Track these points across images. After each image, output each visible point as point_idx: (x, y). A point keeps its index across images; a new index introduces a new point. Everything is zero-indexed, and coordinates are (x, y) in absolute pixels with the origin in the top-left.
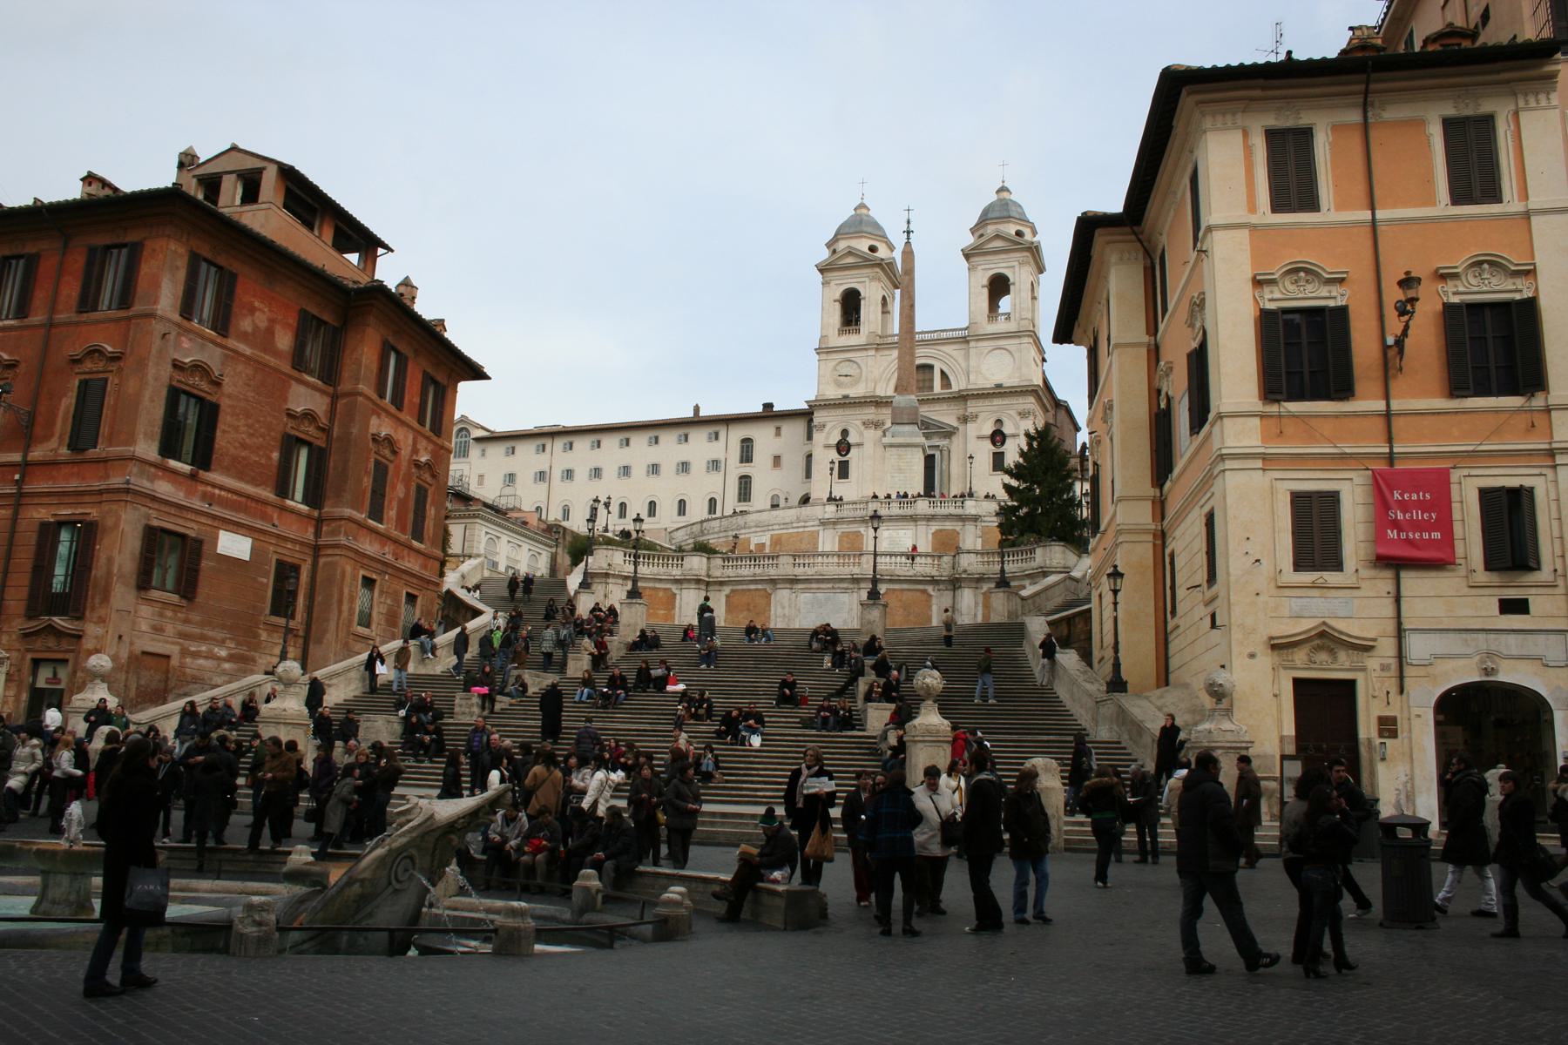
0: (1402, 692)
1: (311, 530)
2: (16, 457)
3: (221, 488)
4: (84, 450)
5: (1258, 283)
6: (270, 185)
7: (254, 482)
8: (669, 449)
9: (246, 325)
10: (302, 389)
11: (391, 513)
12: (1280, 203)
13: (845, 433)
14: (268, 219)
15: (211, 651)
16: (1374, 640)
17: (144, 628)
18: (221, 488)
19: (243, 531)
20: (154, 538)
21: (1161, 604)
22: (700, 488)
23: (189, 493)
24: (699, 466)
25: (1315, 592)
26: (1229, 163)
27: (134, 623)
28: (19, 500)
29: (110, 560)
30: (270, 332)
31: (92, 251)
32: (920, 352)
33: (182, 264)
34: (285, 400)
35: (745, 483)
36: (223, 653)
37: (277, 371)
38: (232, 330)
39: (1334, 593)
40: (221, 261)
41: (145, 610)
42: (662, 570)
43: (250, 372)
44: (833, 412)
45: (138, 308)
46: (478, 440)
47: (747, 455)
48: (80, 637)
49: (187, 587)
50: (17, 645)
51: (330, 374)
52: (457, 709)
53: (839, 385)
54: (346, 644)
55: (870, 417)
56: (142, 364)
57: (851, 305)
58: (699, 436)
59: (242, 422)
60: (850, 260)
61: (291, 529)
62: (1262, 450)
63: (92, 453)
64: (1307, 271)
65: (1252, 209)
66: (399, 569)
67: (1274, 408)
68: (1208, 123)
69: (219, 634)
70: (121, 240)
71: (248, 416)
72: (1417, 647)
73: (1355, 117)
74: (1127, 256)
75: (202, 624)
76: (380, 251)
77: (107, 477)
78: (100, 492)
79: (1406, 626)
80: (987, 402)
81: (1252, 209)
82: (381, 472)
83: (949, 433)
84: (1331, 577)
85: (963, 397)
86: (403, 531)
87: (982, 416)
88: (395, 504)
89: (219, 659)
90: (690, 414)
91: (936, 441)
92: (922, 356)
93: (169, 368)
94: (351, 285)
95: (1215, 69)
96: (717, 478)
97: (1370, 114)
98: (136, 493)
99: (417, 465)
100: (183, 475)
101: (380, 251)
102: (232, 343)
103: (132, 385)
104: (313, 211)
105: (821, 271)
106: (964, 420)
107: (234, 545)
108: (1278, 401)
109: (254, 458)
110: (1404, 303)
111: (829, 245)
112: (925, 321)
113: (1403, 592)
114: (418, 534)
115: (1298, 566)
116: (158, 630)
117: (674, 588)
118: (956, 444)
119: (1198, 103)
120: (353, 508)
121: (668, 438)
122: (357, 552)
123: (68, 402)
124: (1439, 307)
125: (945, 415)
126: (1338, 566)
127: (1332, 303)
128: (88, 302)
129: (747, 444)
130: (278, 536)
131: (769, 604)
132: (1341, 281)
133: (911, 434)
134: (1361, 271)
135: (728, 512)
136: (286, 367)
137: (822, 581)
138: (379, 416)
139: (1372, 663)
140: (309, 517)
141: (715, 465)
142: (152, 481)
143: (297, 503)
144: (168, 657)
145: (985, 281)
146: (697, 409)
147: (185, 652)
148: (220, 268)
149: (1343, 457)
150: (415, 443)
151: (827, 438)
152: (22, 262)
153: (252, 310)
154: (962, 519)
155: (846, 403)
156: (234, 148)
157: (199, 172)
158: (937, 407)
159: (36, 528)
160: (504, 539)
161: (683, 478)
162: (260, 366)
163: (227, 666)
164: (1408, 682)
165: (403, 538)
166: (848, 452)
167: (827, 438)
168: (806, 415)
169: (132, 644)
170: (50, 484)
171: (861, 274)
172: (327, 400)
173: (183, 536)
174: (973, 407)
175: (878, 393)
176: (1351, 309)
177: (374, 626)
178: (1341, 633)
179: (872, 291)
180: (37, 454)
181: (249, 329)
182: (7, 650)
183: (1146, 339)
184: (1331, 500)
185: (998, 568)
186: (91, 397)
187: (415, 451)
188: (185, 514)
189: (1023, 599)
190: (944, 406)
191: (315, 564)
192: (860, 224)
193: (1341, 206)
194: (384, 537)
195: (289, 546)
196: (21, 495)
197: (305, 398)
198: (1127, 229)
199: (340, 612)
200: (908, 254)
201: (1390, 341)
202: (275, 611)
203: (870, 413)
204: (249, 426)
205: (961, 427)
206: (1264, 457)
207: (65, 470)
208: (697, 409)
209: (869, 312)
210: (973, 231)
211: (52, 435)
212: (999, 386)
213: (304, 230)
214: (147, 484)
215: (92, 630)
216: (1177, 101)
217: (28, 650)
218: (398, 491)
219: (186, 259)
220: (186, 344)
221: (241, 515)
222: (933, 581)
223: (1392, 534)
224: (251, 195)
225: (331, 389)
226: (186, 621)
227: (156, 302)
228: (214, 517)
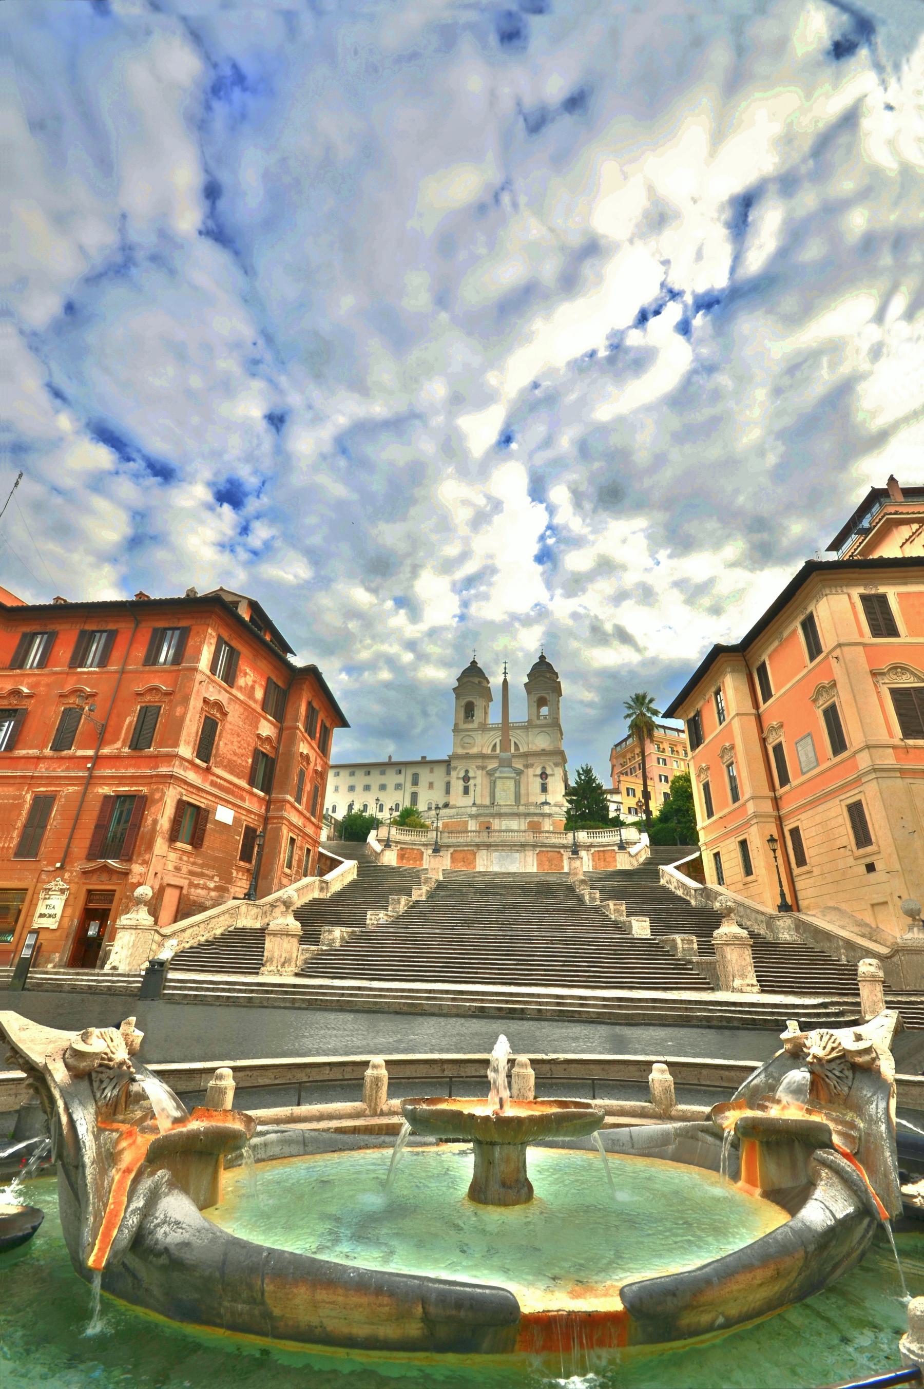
1: (264, 807)
2: (90, 753)
7: (239, 777)
9: (241, 681)
11: (304, 800)
13: (544, 768)
15: (205, 884)
18: (221, 778)
19: (230, 806)
20: (182, 806)
23: (204, 780)
29: (155, 822)
30: (253, 688)
31: (155, 630)
33: (214, 641)
36: (212, 885)
40: (234, 643)
41: (173, 856)
42: (417, 838)
43: (242, 710)
47: (415, 782)
49: (196, 840)
52: (368, 922)
59: (235, 740)
64: (900, 667)
71: (238, 735)
75: (202, 866)
77: (157, 767)
78: (151, 777)
85: (526, 755)
89: (209, 889)
90: (387, 760)
102: (234, 691)
103: (179, 711)
106: (527, 766)
107: (225, 815)
109: (239, 761)
117: (422, 848)
121: (375, 773)
123: (130, 720)
131: (475, 858)
133: (509, 772)
136: (259, 710)
137: (505, 846)
140: (263, 799)
144: (181, 888)
146: (390, 757)
147: (191, 885)
152: (105, 635)
153: (246, 674)
154: (543, 815)
155: (467, 757)
159: (101, 799)
163: (213, 894)
165: (308, 815)
173: (198, 808)
180: (105, 751)
181: (243, 685)
182: (68, 883)
183: (754, 711)
185: (619, 838)
196: (91, 777)
202: (242, 859)
203: (479, 762)
204: (239, 742)
206: (901, 771)
207: (126, 762)
208: (390, 757)
211: (118, 740)
214: (182, 772)
215: (137, 869)
217: (84, 883)
219: (215, 640)
220: (211, 689)
222: (564, 847)
226: (194, 864)
227: (198, 661)
228: (216, 797)
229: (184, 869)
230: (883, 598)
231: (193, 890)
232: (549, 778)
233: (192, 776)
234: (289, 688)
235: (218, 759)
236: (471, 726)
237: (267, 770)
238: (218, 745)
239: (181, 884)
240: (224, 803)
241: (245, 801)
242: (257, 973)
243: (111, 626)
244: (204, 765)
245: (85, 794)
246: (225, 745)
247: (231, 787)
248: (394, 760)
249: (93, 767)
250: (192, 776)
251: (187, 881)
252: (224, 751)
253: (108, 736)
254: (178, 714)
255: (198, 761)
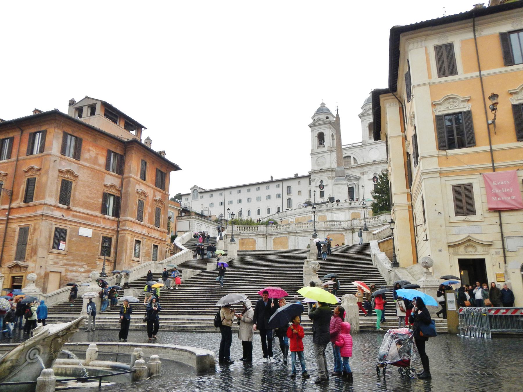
0: (505, 263)
3: (80, 212)
4: (28, 202)
5: (434, 105)
6: (99, 110)
7: (93, 210)
8: (264, 191)
10: (109, 177)
11: (146, 218)
12: (442, 73)
13: (322, 181)
14: (100, 122)
16: (491, 242)
17: (51, 262)
18: (80, 212)
19: (89, 227)
21: (413, 233)
22: (275, 204)
24: (274, 197)
25: (465, 224)
26: (420, 58)
27: (47, 261)
28: (8, 221)
30: (96, 158)
32: (344, 152)
34: (104, 181)
35: (289, 201)
37: (99, 171)
38: (81, 158)
39: (472, 224)
41: (51, 257)
42: (251, 232)
43: (89, 172)
44: (317, 175)
45: (45, 153)
46: (200, 193)
47: (289, 192)
48: (27, 267)
50: (7, 272)
51: (120, 170)
53: (319, 165)
54: (129, 264)
55: (330, 176)
56: (47, 172)
57: (321, 137)
58: (273, 186)
60: (320, 122)
61: (108, 225)
62: (439, 170)
63: (31, 203)
64: (452, 98)
65: (430, 77)
66: (150, 237)
67: (443, 153)
68: (411, 46)
69: (80, 263)
70: (40, 130)
71: (89, 187)
72: (510, 244)
73: (471, 35)
74: (392, 104)
75: (74, 260)
76: (143, 129)
77: (36, 211)
78: (34, 216)
79: (505, 235)
80: (370, 167)
81: (430, 77)
82: (141, 205)
83: (358, 179)
84: (471, 218)
85: (362, 166)
86: (151, 223)
87: (369, 172)
88: (147, 215)
89: (81, 272)
90: (269, 179)
91: (353, 182)
92: (345, 154)
93: (58, 172)
94: (126, 140)
95: (411, 25)
96: (280, 200)
97: (476, 34)
98: (46, 216)
99: (155, 200)
100: (64, 209)
101: (143, 129)
102: (81, 162)
103: (44, 179)
104: (117, 117)
105: (310, 127)
106: (363, 174)
107: (85, 232)
108: (445, 150)
109: (92, 201)
110: (493, 105)
111: (312, 118)
112: (346, 141)
113: (503, 222)
114: (157, 224)
115: (457, 214)
116: (56, 263)
117: (255, 238)
118: (361, 183)
119: (407, 39)
120: (130, 217)
121: (263, 188)
122: (132, 232)
123: (23, 187)
124: (510, 107)
125: (356, 173)
126: (474, 213)
127: (465, 110)
128: (30, 152)
129: (289, 188)
130: (103, 228)
132: (468, 100)
134: (477, 95)
135: (284, 210)
136: (103, 170)
138: (139, 184)
139: (492, 251)
140: (114, 221)
141: (278, 196)
142: (52, 212)
143: (110, 216)
144: (61, 273)
145: (367, 125)
146: (272, 177)
147: (67, 271)
148: (76, 137)
149: (473, 170)
150: (154, 192)
151: (316, 184)
153: (89, 151)
155: (321, 171)
156: (87, 97)
157: (76, 106)
158: (353, 170)
160: (204, 225)
161: (269, 201)
162: (92, 169)
163: (84, 274)
164: (507, 258)
165: (151, 226)
166: (323, 188)
167: (316, 184)
168: (309, 177)
169: (46, 269)
170: (18, 215)
171: (325, 126)
172: (120, 180)
174: (366, 169)
175: (332, 167)
176: (472, 111)
177: (140, 257)
178: (477, 240)
179: (328, 133)
180: (14, 205)
181: (88, 157)
183: (401, 134)
184: (469, 187)
186: (31, 183)
187: (154, 196)
188: (66, 222)
189: (374, 235)
190: (356, 170)
191: (117, 237)
192: (322, 110)
193: (466, 72)
194: (144, 226)
195: (107, 231)
196: (8, 219)
197: (111, 179)
198: (391, 94)
199: (126, 253)
200: (338, 117)
201: (490, 122)
203: (330, 174)
204: (90, 191)
205: (362, 177)
206: (441, 172)
207: (23, 209)
208: (272, 177)
209: (328, 140)
210: (362, 108)
211: (18, 198)
212: (374, 161)
213: (115, 125)
216: (399, 40)
218: (148, 210)
221: (88, 222)
223: (494, 199)
224: (93, 113)
225: (121, 176)
227: (51, 150)
228: (78, 223)
229: (61, 263)
230: (450, 47)
231: (69, 273)
232: (325, 187)
233: (57, 214)
234: (125, 154)
235: (76, 202)
236: (323, 149)
237: (114, 204)
238: (74, 194)
239: (60, 271)
240: (82, 226)
241: (100, 223)
242: (80, 313)
243: (11, 135)
244: (66, 207)
245: (6, 228)
246: (78, 193)
247: (89, 216)
248: (274, 179)
249: (8, 215)
250: (57, 214)
251: (64, 269)
252: (80, 197)
253: (14, 197)
254: (43, 181)
255: (60, 205)
